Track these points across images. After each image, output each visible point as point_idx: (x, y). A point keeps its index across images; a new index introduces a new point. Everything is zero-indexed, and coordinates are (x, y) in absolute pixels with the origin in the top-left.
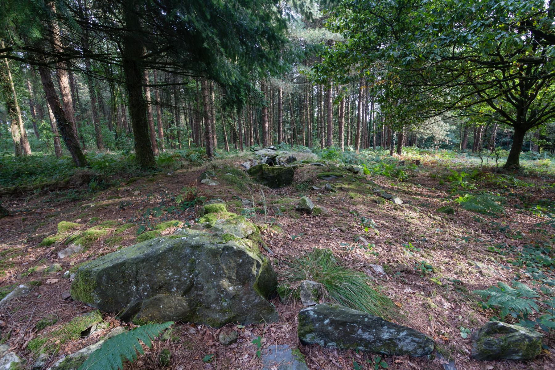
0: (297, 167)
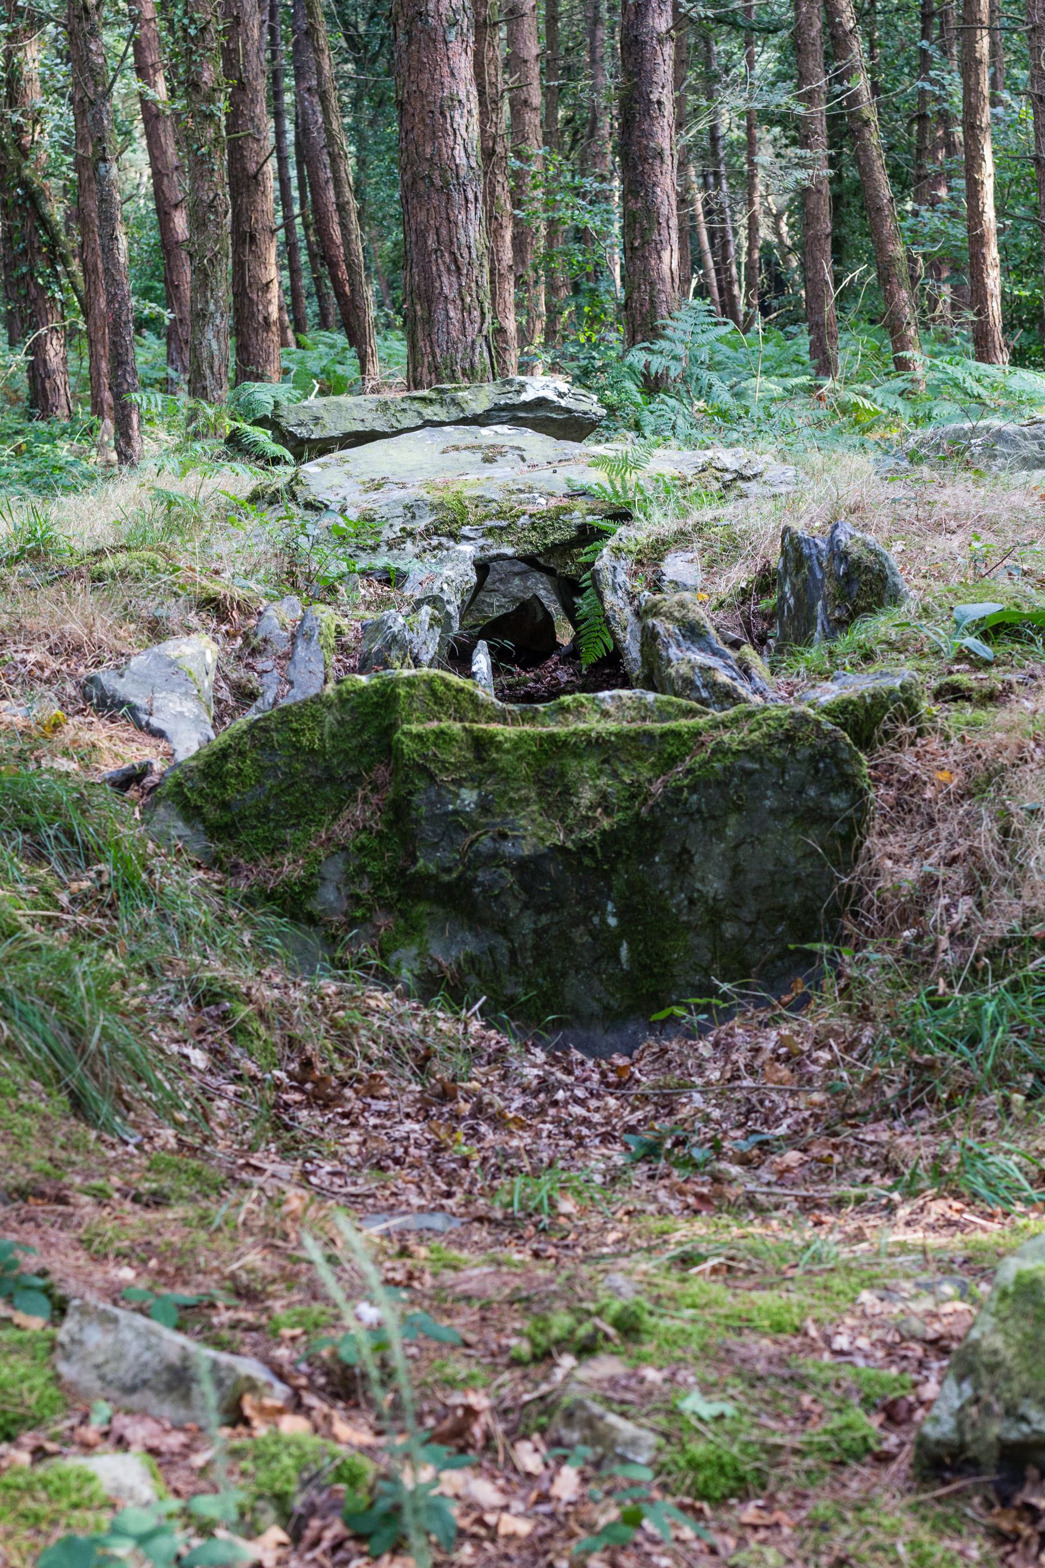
0: (905, 705)
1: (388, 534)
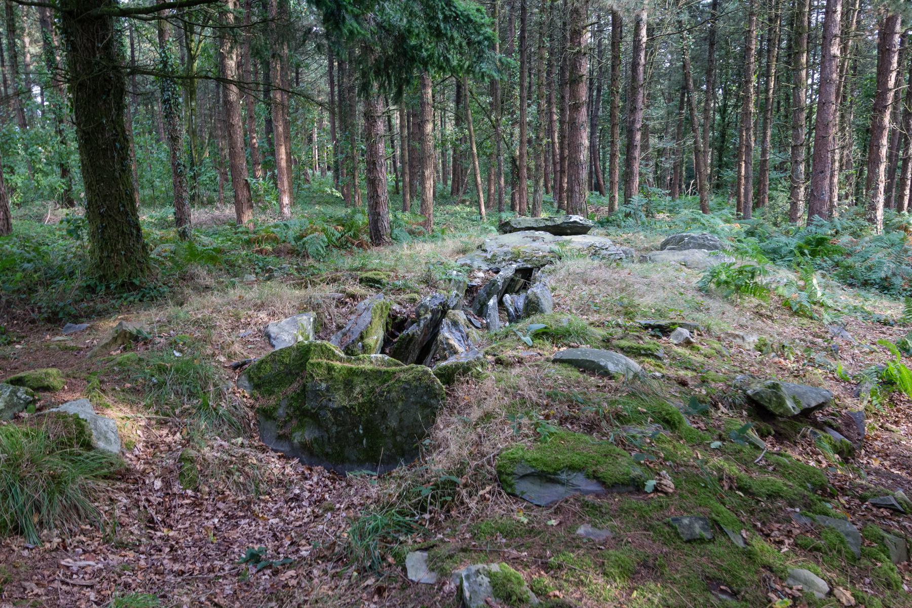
1: (499, 260)
